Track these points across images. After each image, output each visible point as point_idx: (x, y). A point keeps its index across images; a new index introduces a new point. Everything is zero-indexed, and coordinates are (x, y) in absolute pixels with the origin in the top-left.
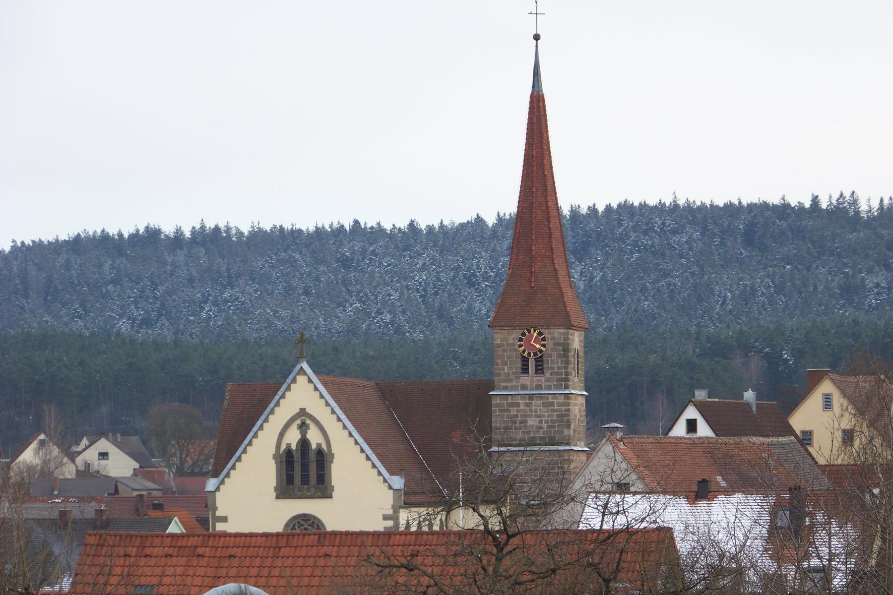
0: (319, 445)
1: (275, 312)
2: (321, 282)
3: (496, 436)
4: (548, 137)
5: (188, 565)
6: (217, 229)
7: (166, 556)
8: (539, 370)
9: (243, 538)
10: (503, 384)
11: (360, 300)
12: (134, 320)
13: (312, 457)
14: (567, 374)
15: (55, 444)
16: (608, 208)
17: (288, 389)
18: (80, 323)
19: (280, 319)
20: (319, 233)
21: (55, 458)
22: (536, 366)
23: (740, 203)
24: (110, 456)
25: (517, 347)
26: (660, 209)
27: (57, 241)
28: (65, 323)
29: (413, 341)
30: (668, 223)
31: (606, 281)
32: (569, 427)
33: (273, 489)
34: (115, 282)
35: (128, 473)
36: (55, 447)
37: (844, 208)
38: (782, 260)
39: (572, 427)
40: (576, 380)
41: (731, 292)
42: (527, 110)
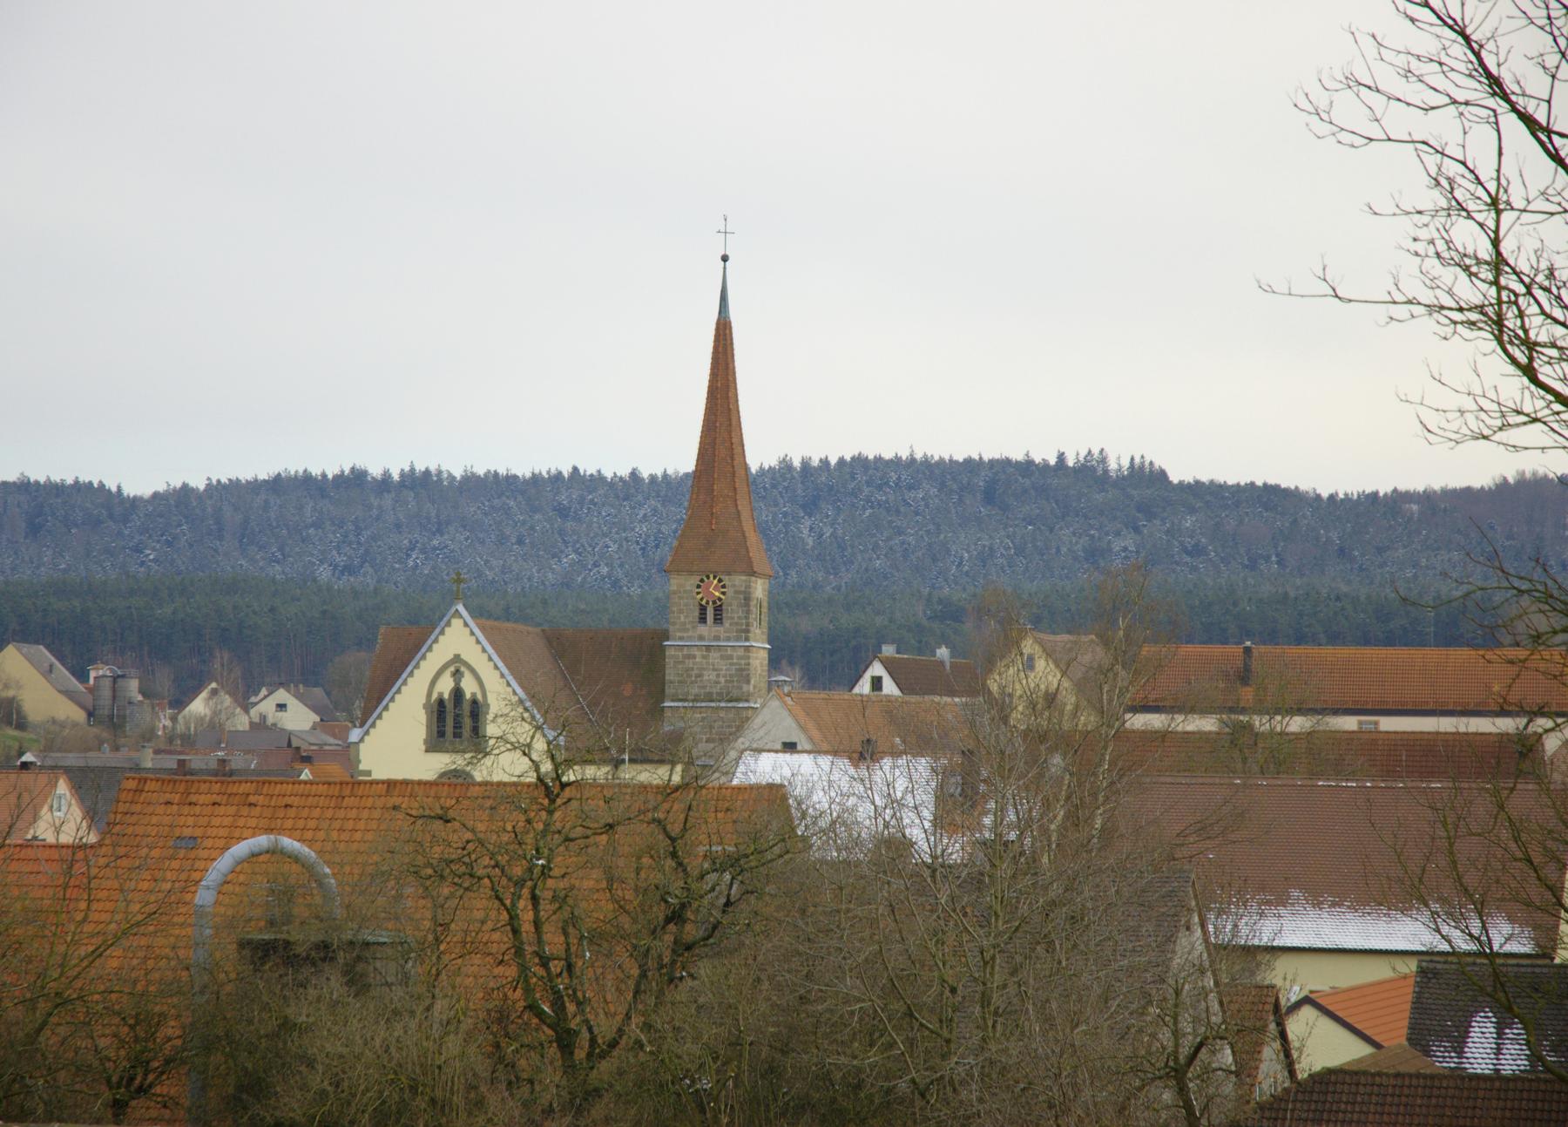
0: (474, 694)
1: (487, 562)
2: (535, 531)
3: (669, 691)
4: (734, 368)
5: (237, 815)
6: (427, 473)
7: (214, 804)
8: (718, 619)
9: (302, 786)
10: (678, 634)
11: (576, 551)
12: (336, 566)
13: (466, 708)
14: (748, 625)
15: (228, 693)
16: (841, 461)
17: (442, 632)
18: (278, 568)
19: (491, 569)
20: (536, 479)
21: (226, 709)
22: (715, 615)
23: (981, 458)
24: (288, 708)
25: (694, 594)
26: (896, 463)
27: (256, 480)
28: (261, 568)
29: (629, 595)
30: (903, 477)
31: (836, 538)
32: (748, 682)
33: (422, 742)
34: (317, 525)
35: (307, 726)
36: (227, 696)
37: (1093, 466)
38: (1024, 520)
39: (752, 682)
40: (758, 631)
41: (968, 552)
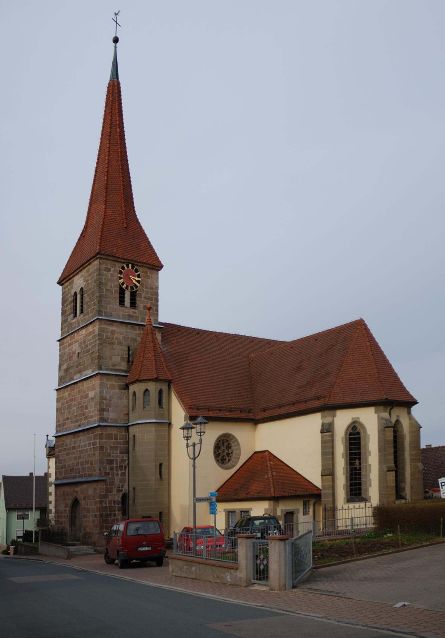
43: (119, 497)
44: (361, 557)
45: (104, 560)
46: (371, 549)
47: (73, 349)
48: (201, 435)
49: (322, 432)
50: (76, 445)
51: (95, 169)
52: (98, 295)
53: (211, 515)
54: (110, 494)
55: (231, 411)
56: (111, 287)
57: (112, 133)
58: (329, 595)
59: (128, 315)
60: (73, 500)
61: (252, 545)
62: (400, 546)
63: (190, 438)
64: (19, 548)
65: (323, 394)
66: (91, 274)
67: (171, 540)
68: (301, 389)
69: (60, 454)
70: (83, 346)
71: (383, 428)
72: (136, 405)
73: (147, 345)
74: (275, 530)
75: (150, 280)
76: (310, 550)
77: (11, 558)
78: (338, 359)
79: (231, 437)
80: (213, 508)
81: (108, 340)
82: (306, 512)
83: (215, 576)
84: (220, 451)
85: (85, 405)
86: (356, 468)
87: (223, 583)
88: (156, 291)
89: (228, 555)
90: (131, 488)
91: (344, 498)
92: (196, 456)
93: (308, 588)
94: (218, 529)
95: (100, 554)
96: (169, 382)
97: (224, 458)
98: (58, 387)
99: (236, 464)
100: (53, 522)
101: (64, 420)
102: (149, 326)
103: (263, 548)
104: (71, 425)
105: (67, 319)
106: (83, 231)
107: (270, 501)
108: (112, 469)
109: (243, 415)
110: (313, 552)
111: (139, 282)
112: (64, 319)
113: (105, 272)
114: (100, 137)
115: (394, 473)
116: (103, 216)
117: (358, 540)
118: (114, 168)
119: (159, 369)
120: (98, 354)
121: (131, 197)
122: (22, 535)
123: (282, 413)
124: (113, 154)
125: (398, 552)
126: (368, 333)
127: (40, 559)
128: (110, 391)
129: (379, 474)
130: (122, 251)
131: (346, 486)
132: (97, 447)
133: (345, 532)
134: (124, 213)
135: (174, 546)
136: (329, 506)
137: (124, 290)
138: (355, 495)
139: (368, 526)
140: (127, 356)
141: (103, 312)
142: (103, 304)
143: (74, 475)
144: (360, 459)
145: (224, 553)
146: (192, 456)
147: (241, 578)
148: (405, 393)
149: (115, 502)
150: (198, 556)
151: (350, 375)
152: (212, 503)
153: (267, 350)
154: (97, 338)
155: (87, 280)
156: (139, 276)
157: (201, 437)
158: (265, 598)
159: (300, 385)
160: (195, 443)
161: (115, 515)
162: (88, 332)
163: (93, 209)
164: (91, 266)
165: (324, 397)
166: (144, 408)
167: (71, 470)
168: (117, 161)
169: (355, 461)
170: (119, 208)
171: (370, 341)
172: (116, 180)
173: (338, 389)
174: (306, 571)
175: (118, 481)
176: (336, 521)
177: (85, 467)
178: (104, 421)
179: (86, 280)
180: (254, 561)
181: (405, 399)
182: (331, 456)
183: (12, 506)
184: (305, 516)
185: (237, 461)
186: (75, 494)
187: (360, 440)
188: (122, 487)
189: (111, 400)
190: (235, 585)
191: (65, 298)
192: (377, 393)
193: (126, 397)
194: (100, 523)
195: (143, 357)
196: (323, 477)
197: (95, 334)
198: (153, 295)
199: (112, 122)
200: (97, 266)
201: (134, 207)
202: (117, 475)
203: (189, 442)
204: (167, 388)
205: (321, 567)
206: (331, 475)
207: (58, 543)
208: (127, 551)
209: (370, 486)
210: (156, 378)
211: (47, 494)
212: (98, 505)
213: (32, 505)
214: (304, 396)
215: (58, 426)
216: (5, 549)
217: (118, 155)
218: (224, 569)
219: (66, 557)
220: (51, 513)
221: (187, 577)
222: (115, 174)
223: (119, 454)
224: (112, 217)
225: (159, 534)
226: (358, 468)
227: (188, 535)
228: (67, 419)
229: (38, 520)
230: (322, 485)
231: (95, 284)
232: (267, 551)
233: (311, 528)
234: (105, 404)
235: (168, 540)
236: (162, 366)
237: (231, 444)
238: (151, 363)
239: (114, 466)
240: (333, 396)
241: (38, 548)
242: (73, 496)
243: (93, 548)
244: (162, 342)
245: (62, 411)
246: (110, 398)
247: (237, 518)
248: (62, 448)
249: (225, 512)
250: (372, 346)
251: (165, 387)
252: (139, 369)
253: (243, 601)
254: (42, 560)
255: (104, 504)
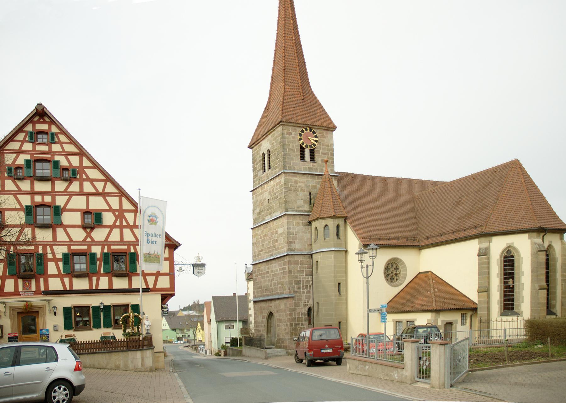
42: (306, 64)
43: (305, 310)
44: (513, 364)
45: (294, 360)
46: (522, 358)
47: (264, 197)
48: (373, 259)
49: (479, 256)
50: (269, 270)
51: (274, 55)
52: (282, 154)
53: (382, 323)
54: (298, 308)
55: (398, 240)
56: (293, 147)
57: (286, 25)
58: (482, 396)
59: (308, 168)
60: (269, 313)
61: (416, 348)
62: (550, 357)
63: (363, 261)
64: (228, 351)
65: (480, 223)
66: (276, 138)
67: (348, 345)
68: (461, 220)
69: (256, 278)
70: (272, 194)
71: (536, 252)
72: (318, 237)
73: (326, 190)
74: (436, 337)
75: (326, 139)
76: (466, 354)
77: (222, 359)
78: (494, 194)
79: (399, 261)
80: (384, 317)
81: (292, 188)
82: (463, 323)
83: (385, 374)
84: (389, 272)
85: (275, 239)
86: (510, 286)
87: (392, 380)
88: (332, 147)
89: (395, 357)
90: (315, 303)
91: (498, 312)
92: (369, 276)
93: (464, 388)
94: (387, 335)
95: (291, 355)
96: (345, 218)
97: (393, 278)
98: (253, 226)
99: (403, 282)
100: (253, 331)
101: (259, 251)
102: (326, 175)
103: (426, 352)
104: (264, 255)
105: (258, 174)
106: (267, 105)
107: (432, 313)
108: (299, 288)
109: (409, 243)
110: (469, 357)
111: (316, 141)
112: (255, 175)
113: (287, 136)
114: (276, 29)
115: (546, 291)
116: (283, 92)
117: (510, 349)
118: (290, 53)
119: (336, 209)
120: (285, 199)
121: (306, 75)
122: (229, 341)
123: (443, 240)
124: (288, 42)
125: (548, 362)
126: (523, 171)
127: (244, 359)
128: (296, 227)
129: (531, 292)
130: (301, 118)
131: (499, 301)
132: (286, 271)
133: (499, 342)
134: (301, 88)
135: (351, 349)
136: (484, 318)
137: (304, 149)
138: (508, 310)
139: (519, 337)
140: (309, 200)
141: (288, 167)
142: (287, 160)
143: (269, 293)
144: (513, 278)
145: (392, 355)
146: (365, 276)
147: (406, 376)
148: (558, 221)
149: (302, 314)
150: (370, 357)
151: (505, 207)
152: (383, 313)
153: (430, 190)
154: (283, 187)
155: (272, 143)
156: (316, 137)
157: (373, 260)
158: (426, 394)
159: (459, 217)
160: (368, 265)
161: (302, 324)
162: (275, 183)
163: (274, 87)
164: (275, 132)
165: (481, 226)
166: (324, 239)
167: (266, 290)
168: (292, 47)
169: (509, 280)
170: (297, 84)
171: (525, 178)
172: (292, 62)
173: (494, 219)
174: (463, 373)
175: (305, 297)
176: (490, 331)
177: (277, 287)
178: (291, 251)
179: (271, 143)
180: (418, 362)
181: (558, 226)
182: (487, 276)
183: (221, 319)
184: (462, 326)
185: (404, 280)
186: (270, 308)
187: (514, 262)
188: (308, 302)
189: (297, 235)
190: (401, 382)
191: (255, 158)
192: (531, 222)
193: (309, 232)
194: (290, 331)
195: (323, 200)
196: (480, 293)
197: (281, 184)
198: (329, 151)
199: (286, 15)
200: (280, 131)
201: (309, 83)
202: (304, 292)
203: (363, 264)
204: (344, 223)
205: (476, 370)
206: (487, 292)
207: (257, 347)
208: (312, 352)
209: (523, 302)
210: (334, 215)
211: (247, 309)
212: (289, 317)
213: (236, 318)
214: (463, 226)
215: (254, 256)
216: (217, 352)
217: (293, 42)
218: (392, 368)
219: (264, 357)
220: (251, 324)
221: (362, 374)
222: (291, 57)
223: (304, 276)
224: (290, 92)
225: (338, 339)
226: (511, 286)
227: (362, 340)
228: (262, 250)
229: (241, 329)
230: (478, 300)
231: (280, 145)
232: (429, 354)
233: (468, 336)
234: (292, 238)
235: (346, 345)
236: (339, 206)
237: (399, 266)
238: (330, 204)
239: (301, 286)
240: (490, 225)
241: (242, 351)
242: (268, 310)
243: (285, 351)
244: (338, 187)
245: (257, 245)
246: (295, 233)
247: (403, 327)
248: (258, 273)
249: (394, 322)
250: (526, 181)
251: (341, 222)
252: (320, 209)
253: (408, 396)
254: (246, 360)
255: (293, 316)
